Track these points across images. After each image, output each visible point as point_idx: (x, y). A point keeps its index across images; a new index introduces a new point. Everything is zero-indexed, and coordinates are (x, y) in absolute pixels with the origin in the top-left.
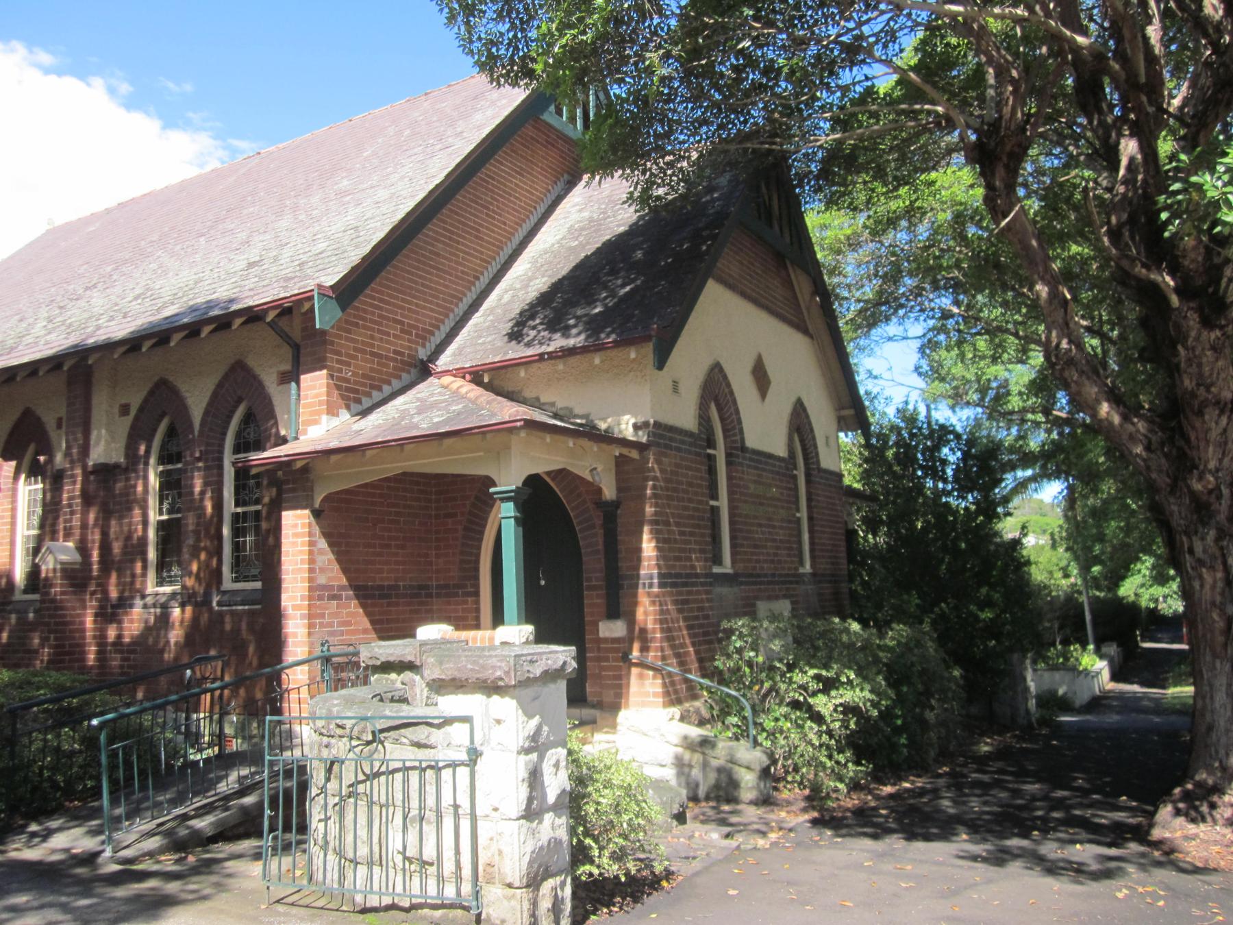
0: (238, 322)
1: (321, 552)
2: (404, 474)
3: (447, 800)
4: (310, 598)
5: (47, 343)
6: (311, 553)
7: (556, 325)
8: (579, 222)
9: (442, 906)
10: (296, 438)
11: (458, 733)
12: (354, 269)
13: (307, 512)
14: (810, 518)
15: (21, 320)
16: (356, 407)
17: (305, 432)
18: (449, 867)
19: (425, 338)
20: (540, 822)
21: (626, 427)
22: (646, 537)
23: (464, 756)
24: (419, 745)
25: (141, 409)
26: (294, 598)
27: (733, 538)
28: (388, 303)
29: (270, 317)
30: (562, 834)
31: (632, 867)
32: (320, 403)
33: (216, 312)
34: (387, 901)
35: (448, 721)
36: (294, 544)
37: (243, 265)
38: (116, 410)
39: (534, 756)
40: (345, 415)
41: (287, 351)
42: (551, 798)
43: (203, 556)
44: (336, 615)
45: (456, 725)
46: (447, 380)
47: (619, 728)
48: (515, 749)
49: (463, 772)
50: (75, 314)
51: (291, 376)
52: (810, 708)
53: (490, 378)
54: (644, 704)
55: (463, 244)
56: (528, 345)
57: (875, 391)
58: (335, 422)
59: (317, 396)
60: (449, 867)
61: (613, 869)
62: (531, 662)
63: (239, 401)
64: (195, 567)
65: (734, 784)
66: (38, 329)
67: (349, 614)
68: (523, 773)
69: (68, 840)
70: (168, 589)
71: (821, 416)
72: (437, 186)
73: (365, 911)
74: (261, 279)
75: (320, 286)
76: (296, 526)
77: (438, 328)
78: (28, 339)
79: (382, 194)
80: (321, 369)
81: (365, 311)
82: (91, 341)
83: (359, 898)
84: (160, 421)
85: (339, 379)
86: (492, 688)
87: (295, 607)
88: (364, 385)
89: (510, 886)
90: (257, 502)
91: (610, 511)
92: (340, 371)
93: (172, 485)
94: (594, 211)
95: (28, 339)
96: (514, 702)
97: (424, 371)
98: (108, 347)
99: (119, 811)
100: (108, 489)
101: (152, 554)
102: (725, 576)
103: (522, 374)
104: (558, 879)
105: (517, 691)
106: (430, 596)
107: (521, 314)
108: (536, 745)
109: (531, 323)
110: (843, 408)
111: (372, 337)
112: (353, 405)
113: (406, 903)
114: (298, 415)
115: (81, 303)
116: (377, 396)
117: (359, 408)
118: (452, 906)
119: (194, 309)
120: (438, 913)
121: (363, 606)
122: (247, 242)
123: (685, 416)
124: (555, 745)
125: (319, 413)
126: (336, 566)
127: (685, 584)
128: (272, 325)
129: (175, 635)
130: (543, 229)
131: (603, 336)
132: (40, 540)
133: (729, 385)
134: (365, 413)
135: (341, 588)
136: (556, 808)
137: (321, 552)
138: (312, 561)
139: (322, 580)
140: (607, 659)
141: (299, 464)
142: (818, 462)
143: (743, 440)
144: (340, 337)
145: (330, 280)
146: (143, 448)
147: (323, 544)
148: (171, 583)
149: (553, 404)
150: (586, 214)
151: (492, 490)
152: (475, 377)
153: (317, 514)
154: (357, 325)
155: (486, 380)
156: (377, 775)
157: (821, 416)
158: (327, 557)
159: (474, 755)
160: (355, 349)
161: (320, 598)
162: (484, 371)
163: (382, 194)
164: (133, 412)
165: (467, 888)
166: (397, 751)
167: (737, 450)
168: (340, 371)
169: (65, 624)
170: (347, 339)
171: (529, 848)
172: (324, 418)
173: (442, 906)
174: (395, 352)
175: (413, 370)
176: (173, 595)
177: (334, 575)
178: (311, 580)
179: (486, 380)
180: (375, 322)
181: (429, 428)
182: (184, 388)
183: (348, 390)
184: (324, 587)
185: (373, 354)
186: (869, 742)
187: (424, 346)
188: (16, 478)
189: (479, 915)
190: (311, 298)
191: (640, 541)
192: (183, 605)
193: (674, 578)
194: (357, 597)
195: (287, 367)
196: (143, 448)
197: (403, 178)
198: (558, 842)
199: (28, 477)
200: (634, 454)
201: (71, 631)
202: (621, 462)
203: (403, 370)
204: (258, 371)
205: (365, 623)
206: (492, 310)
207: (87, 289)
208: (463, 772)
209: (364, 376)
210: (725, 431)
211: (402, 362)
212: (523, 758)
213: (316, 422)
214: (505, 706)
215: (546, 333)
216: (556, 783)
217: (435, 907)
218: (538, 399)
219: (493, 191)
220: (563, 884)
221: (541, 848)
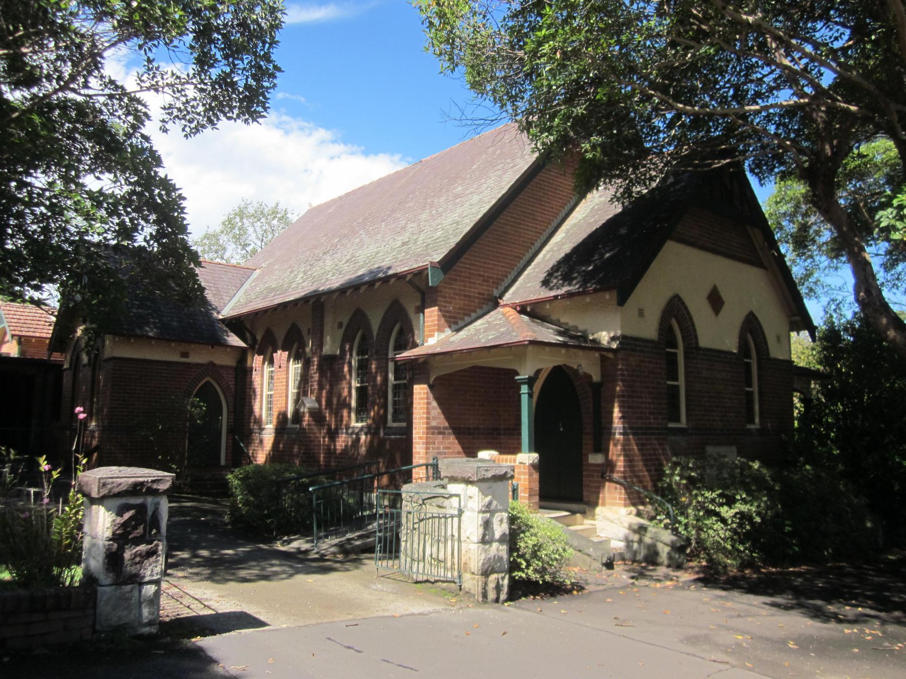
0: (393, 280)
1: (434, 408)
2: (474, 367)
3: (449, 533)
4: (427, 433)
5: (303, 288)
6: (428, 408)
7: (567, 278)
8: (597, 204)
9: (447, 581)
10: (423, 344)
11: (454, 501)
12: (451, 251)
13: (426, 386)
14: (760, 392)
15: (291, 272)
16: (454, 327)
17: (427, 341)
18: (449, 564)
19: (498, 284)
20: (491, 546)
21: (604, 337)
22: (616, 405)
23: (456, 513)
24: (439, 507)
25: (348, 325)
26: (419, 433)
27: (687, 405)
28: (475, 265)
29: (408, 278)
30: (505, 555)
31: (548, 578)
32: (434, 325)
33: (381, 275)
34: (425, 578)
35: (451, 496)
36: (419, 403)
37: (399, 243)
38: (336, 325)
39: (488, 515)
40: (448, 332)
41: (418, 295)
42: (497, 535)
43: (376, 408)
44: (441, 443)
45: (454, 498)
46: (508, 309)
47: (597, 517)
48: (477, 509)
49: (456, 520)
50: (317, 271)
51: (421, 310)
52: (717, 514)
53: (532, 311)
54: (614, 504)
55: (524, 225)
56: (551, 289)
57: (840, 298)
58: (443, 336)
59: (433, 321)
60: (449, 564)
61: (534, 577)
62: (487, 470)
63: (396, 323)
64: (372, 414)
65: (656, 553)
66: (299, 279)
67: (449, 443)
68: (480, 522)
69: (299, 544)
70: (360, 425)
71: (771, 319)
72: (504, 195)
73: (417, 582)
74: (407, 254)
75: (431, 263)
76: (420, 391)
77: (506, 277)
78: (294, 285)
79: (476, 198)
80: (435, 306)
81: (462, 272)
82: (321, 289)
83: (415, 577)
84: (357, 332)
85: (445, 311)
86: (468, 482)
87: (420, 438)
88: (459, 313)
89: (473, 573)
90: (405, 378)
91: (597, 388)
92: (446, 307)
93: (363, 367)
94: (597, 207)
95: (294, 285)
96: (477, 489)
97: (496, 305)
98: (330, 293)
99: (322, 534)
100: (330, 368)
101: (353, 404)
102: (681, 431)
103: (548, 307)
104: (501, 575)
105: (479, 484)
106: (500, 434)
107: (552, 268)
108: (488, 509)
109: (556, 274)
110: (794, 315)
111: (465, 286)
112: (453, 326)
113: (432, 580)
114: (423, 331)
115: (321, 263)
116: (467, 319)
117: (457, 327)
118: (450, 582)
119: (371, 272)
120: (445, 584)
121: (457, 438)
122: (404, 228)
123: (649, 330)
124: (501, 511)
125: (434, 331)
126: (442, 416)
127: (645, 434)
128: (410, 282)
129: (363, 450)
130: (577, 209)
131: (589, 285)
132: (298, 394)
133: (686, 308)
134: (458, 330)
135: (445, 428)
136: (501, 540)
137: (434, 408)
138: (428, 413)
139: (434, 424)
140: (593, 476)
141: (421, 360)
142: (768, 354)
143: (697, 343)
144: (446, 288)
145: (437, 258)
146: (347, 346)
147: (434, 404)
148: (362, 421)
149: (567, 324)
150: (603, 199)
151: (517, 378)
152: (522, 309)
153: (431, 387)
154: (456, 280)
155: (529, 309)
156: (422, 520)
157: (771, 319)
158: (436, 411)
159: (461, 512)
160: (454, 294)
161: (433, 433)
162: (527, 305)
163: (476, 198)
164: (344, 327)
165: (456, 574)
166: (431, 509)
167: (693, 349)
168: (446, 307)
169: (311, 441)
170: (450, 288)
171: (483, 557)
172: (436, 333)
173: (447, 581)
174: (479, 293)
175: (490, 303)
176: (362, 429)
177: (440, 420)
178: (427, 423)
179: (529, 309)
180: (466, 277)
181: (485, 342)
182: (369, 313)
183: (450, 317)
184: (434, 428)
185: (465, 295)
186: (749, 533)
187: (497, 288)
188: (288, 361)
189: (460, 586)
190: (427, 269)
191: (613, 407)
192: (366, 434)
193: (631, 428)
194: (454, 433)
195: (419, 303)
196: (347, 346)
197: (488, 187)
198: (501, 559)
199: (294, 360)
200: (610, 355)
201: (314, 445)
202: (603, 359)
203: (484, 304)
204: (405, 305)
205: (459, 448)
206: (539, 264)
207: (324, 253)
208: (456, 520)
209: (459, 308)
210: (683, 338)
211: (484, 299)
212: (481, 515)
213: (432, 336)
214: (473, 490)
215: (561, 282)
216: (500, 528)
217: (443, 582)
218: (559, 320)
219: (544, 189)
220: (503, 578)
221: (490, 559)
